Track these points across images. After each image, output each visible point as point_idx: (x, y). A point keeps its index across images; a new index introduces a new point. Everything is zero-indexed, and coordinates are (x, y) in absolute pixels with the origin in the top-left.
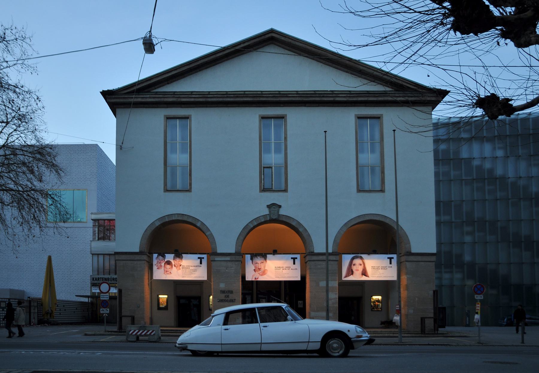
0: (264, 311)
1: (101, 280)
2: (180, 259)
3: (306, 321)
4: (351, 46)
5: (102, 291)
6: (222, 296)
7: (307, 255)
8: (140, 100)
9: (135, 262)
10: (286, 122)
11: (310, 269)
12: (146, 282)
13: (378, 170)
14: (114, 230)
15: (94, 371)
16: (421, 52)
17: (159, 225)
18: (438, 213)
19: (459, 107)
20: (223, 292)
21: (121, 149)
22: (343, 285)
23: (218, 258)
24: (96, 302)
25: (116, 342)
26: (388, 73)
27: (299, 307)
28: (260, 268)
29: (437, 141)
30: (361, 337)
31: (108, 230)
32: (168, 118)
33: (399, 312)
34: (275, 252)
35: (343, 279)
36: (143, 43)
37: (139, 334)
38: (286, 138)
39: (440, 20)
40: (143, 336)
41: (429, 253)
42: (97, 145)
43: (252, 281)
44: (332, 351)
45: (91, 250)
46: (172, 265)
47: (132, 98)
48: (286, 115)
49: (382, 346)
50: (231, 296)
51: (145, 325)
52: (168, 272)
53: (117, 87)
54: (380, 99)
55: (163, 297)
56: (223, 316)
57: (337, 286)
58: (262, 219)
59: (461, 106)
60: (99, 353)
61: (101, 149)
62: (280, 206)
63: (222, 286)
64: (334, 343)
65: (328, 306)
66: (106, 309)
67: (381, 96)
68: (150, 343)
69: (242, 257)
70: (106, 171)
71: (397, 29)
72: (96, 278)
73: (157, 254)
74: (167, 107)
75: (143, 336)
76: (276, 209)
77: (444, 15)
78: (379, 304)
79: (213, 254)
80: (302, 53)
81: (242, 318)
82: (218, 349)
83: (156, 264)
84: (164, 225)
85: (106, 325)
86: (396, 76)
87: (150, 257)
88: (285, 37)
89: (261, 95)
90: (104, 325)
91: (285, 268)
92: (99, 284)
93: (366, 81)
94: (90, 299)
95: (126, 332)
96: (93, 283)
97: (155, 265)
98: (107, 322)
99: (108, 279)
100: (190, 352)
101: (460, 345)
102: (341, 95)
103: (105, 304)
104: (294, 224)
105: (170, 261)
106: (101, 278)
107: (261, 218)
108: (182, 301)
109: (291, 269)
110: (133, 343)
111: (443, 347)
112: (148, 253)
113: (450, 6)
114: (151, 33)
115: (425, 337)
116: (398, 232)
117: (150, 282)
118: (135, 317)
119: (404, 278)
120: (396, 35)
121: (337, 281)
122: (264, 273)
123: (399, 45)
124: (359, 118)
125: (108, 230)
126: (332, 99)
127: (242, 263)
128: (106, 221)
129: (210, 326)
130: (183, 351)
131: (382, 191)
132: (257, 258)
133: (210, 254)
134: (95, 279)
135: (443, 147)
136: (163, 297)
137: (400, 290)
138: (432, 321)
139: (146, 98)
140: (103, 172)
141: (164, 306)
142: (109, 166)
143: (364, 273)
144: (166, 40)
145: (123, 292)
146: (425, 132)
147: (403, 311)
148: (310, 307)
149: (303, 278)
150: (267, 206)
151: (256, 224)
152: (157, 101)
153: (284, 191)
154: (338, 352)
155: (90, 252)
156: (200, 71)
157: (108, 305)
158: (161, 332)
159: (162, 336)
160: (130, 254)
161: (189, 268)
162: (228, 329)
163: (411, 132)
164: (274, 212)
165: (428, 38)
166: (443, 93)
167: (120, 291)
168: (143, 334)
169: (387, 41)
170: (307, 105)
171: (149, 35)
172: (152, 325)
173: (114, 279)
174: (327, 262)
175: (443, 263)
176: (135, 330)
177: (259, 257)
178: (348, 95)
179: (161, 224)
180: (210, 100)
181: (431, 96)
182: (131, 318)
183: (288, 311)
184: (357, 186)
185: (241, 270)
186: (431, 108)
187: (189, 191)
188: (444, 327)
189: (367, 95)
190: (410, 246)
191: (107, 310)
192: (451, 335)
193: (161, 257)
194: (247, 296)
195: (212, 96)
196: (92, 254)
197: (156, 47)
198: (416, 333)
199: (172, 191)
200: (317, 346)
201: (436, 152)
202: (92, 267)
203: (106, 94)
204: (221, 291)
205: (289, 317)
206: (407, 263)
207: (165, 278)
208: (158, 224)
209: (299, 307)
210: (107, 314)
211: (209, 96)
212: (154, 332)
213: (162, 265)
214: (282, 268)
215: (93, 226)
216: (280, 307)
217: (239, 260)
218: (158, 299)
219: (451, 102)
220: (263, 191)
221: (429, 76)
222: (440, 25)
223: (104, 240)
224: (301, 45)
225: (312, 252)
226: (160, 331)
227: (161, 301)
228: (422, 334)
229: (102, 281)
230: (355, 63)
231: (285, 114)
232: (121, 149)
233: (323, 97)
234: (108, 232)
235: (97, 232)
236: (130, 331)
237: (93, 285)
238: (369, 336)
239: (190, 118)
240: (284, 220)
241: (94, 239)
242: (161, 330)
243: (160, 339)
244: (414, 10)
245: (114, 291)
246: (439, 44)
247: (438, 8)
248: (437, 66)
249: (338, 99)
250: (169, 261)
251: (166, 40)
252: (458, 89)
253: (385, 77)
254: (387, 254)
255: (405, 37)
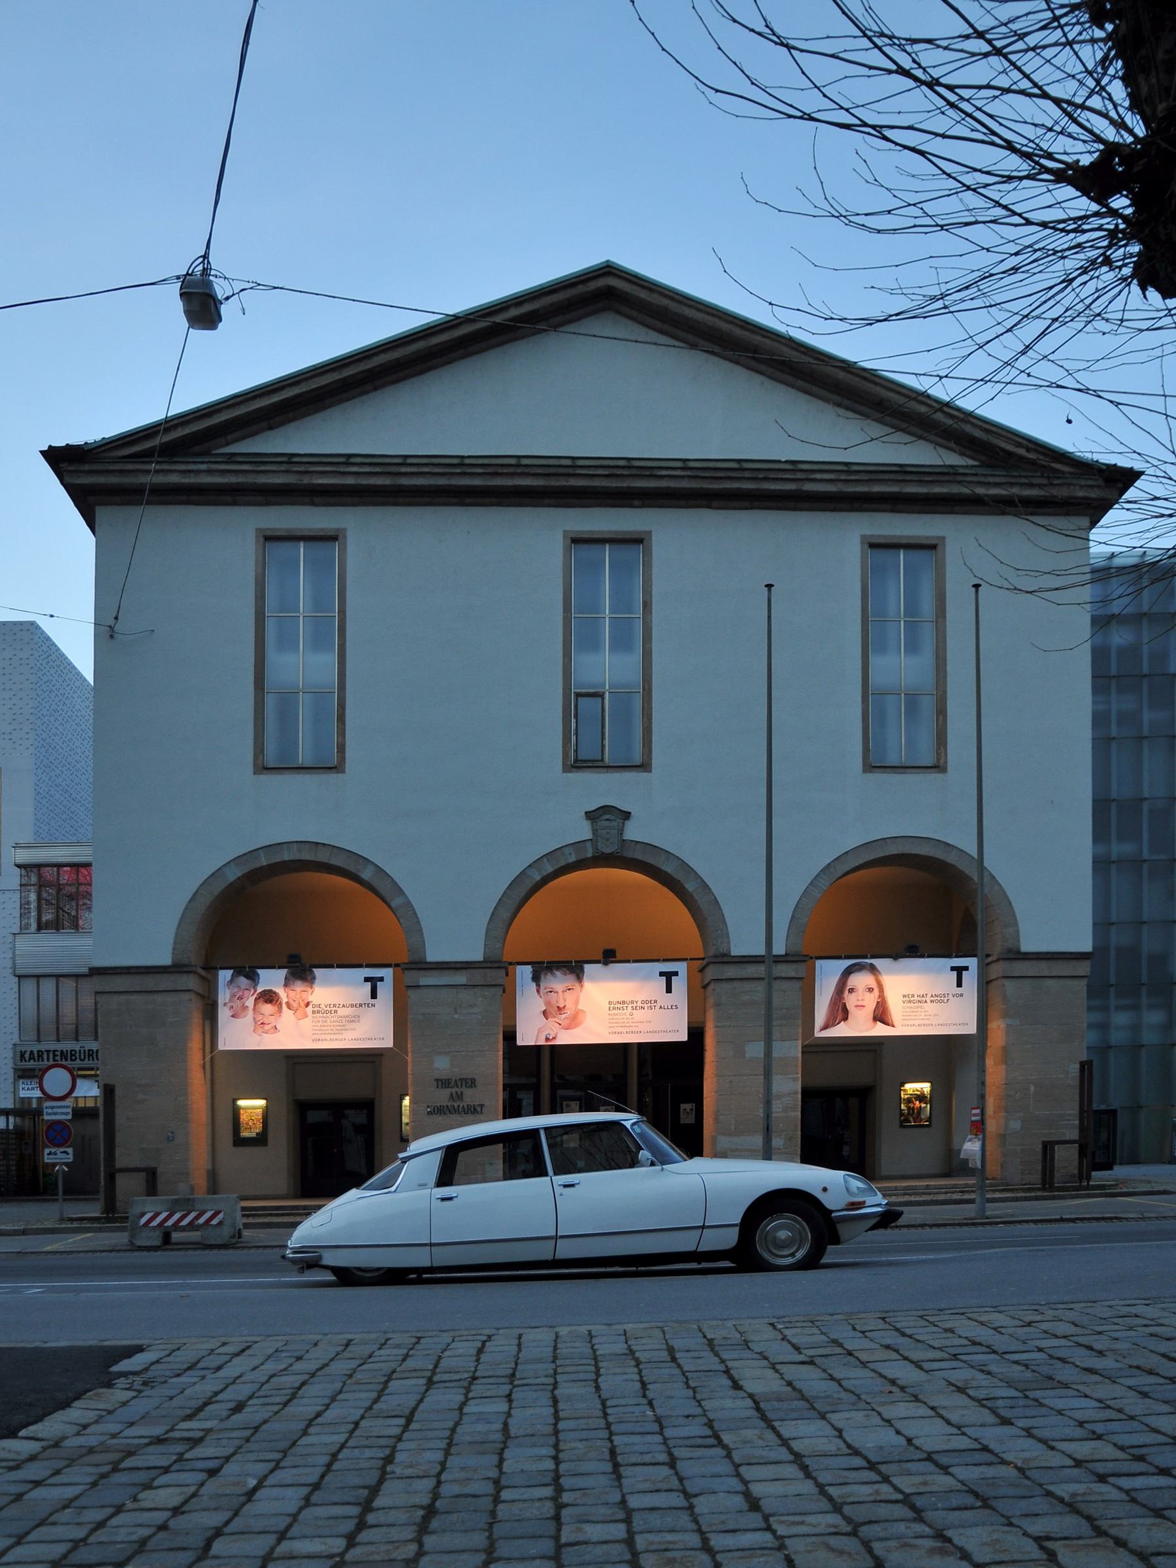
0: (576, 1136)
1: (48, 1060)
2: (306, 984)
3: (696, 1163)
4: (832, 318)
5: (50, 1093)
6: (442, 1097)
7: (708, 964)
8: (174, 479)
9: (159, 998)
10: (648, 553)
11: (718, 1005)
12: (195, 1058)
13: (927, 705)
14: (89, 895)
15: (21, 1345)
16: (1044, 346)
17: (239, 878)
18: (1100, 833)
19: (1157, 517)
20: (443, 1083)
21: (112, 637)
22: (817, 1051)
23: (427, 979)
24: (32, 1129)
25: (95, 1251)
26: (947, 404)
27: (682, 1122)
28: (561, 1006)
29: (1101, 622)
30: (861, 1205)
31: (73, 899)
32: (269, 538)
33: (979, 1127)
34: (609, 957)
35: (818, 1034)
36: (181, 295)
37: (170, 1223)
38: (647, 605)
39: (1101, 251)
40: (183, 1229)
41: (1071, 953)
42: (33, 623)
43: (538, 1048)
44: (776, 1252)
45: (14, 963)
46: (281, 1004)
47: (149, 472)
48: (650, 533)
49: (928, 1229)
50: (471, 1096)
51: (191, 1197)
52: (267, 1027)
53: (98, 437)
54: (937, 490)
55: (252, 1106)
56: (438, 1156)
57: (800, 1055)
58: (570, 854)
59: (1162, 516)
60: (34, 1289)
61: (48, 639)
62: (627, 815)
63: (442, 1065)
64: (781, 1228)
65: (768, 1116)
66: (62, 1150)
67: (943, 482)
68: (206, 1252)
69: (507, 974)
70: (65, 708)
71: (973, 271)
72: (32, 1052)
73: (232, 971)
74: (267, 504)
75: (184, 1231)
76: (614, 824)
77: (1113, 234)
78: (923, 1105)
79: (414, 966)
80: (702, 342)
81: (504, 1162)
82: (420, 1259)
83: (227, 1001)
84: (256, 876)
85: (64, 1200)
86: (969, 417)
87: (208, 981)
88: (651, 290)
89: (570, 471)
90: (57, 1200)
91: (639, 1004)
92: (40, 1070)
93: (876, 429)
94: (11, 1119)
95: (127, 1218)
96: (24, 1070)
97: (225, 1004)
98: (65, 1192)
99: (73, 1055)
100: (329, 1272)
101: (1149, 1218)
102: (818, 476)
103: (59, 1134)
104: (669, 868)
105: (275, 993)
106: (48, 1052)
107: (566, 851)
108: (313, 1117)
109: (658, 1007)
110: (152, 1253)
111: (1103, 1223)
112: (203, 968)
113: (1129, 211)
114: (209, 262)
115: (1054, 1198)
116: (982, 890)
117: (208, 1058)
118: (159, 1170)
119: (997, 1026)
120: (976, 289)
121: (800, 1042)
122: (574, 1021)
123: (979, 322)
124: (873, 546)
125: (71, 897)
126: (791, 486)
127: (504, 992)
128: (65, 869)
129: (395, 1191)
130: (306, 1272)
131: (939, 767)
132: (553, 974)
133: (402, 966)
134: (27, 1056)
135: (1120, 637)
136: (252, 1106)
137: (984, 1065)
138: (1073, 1152)
139: (198, 472)
140: (56, 711)
141: (254, 1135)
142: (75, 692)
143: (881, 1015)
144: (259, 285)
145: (118, 1092)
146: (1057, 589)
147: (991, 1126)
148: (716, 1120)
149: (696, 1033)
150: (586, 813)
151: (550, 869)
152: (232, 484)
153: (640, 769)
154: (793, 1255)
155: (11, 971)
156: (375, 389)
157: (69, 1137)
158: (243, 1216)
159: (246, 1226)
160: (142, 973)
161: (336, 1012)
162: (450, 1199)
163: (1015, 589)
164: (608, 833)
165: (1066, 302)
166: (1121, 479)
167: (109, 1091)
168: (184, 1223)
169: (946, 307)
170: (715, 503)
171: (200, 267)
172: (214, 1193)
173: (91, 1054)
174: (770, 985)
175: (1113, 980)
176: (158, 1210)
177: (558, 973)
178: (843, 477)
179: (244, 875)
180: (405, 481)
181: (1090, 486)
182: (144, 1174)
183: (642, 1135)
184: (864, 753)
185: (501, 1014)
186: (1085, 521)
187: (337, 768)
188: (1111, 1168)
189: (900, 477)
190: (1018, 932)
191: (68, 1154)
192: (1125, 1190)
193: (243, 981)
194: (520, 1095)
195: (414, 470)
196: (19, 977)
197: (224, 309)
198: (1027, 1189)
199: (282, 771)
200: (729, 1239)
201: (1099, 655)
202: (17, 1016)
203: (60, 458)
204: (437, 1080)
205: (644, 1154)
206: (1007, 983)
207: (258, 1045)
208: (233, 875)
209: (682, 1122)
210: (66, 1164)
211: (403, 470)
212: (221, 1216)
213: (246, 1004)
214: (630, 1006)
215: (21, 885)
216: (617, 1124)
217: (497, 983)
218: (236, 1112)
219: (1135, 502)
220: (573, 767)
221: (1069, 421)
222: (1103, 264)
223: (57, 929)
224: (699, 316)
225: (724, 955)
226: (239, 1214)
227: (244, 1117)
228: (1043, 1189)
229: (51, 1060)
230: (865, 379)
231: (647, 529)
232: (112, 637)
233: (766, 479)
234: (74, 903)
235: (33, 906)
236: (143, 1215)
237: (23, 1074)
238: (885, 1202)
239: (340, 538)
240: (639, 856)
241: (24, 928)
242: (243, 1209)
243: (240, 1237)
244: (1024, 215)
245: (88, 1091)
246: (1100, 324)
247: (1096, 214)
248: (1097, 394)
249: (809, 487)
250: (270, 991)
251: (259, 285)
252: (1156, 463)
253: (939, 416)
254: (949, 956)
255: (998, 298)
